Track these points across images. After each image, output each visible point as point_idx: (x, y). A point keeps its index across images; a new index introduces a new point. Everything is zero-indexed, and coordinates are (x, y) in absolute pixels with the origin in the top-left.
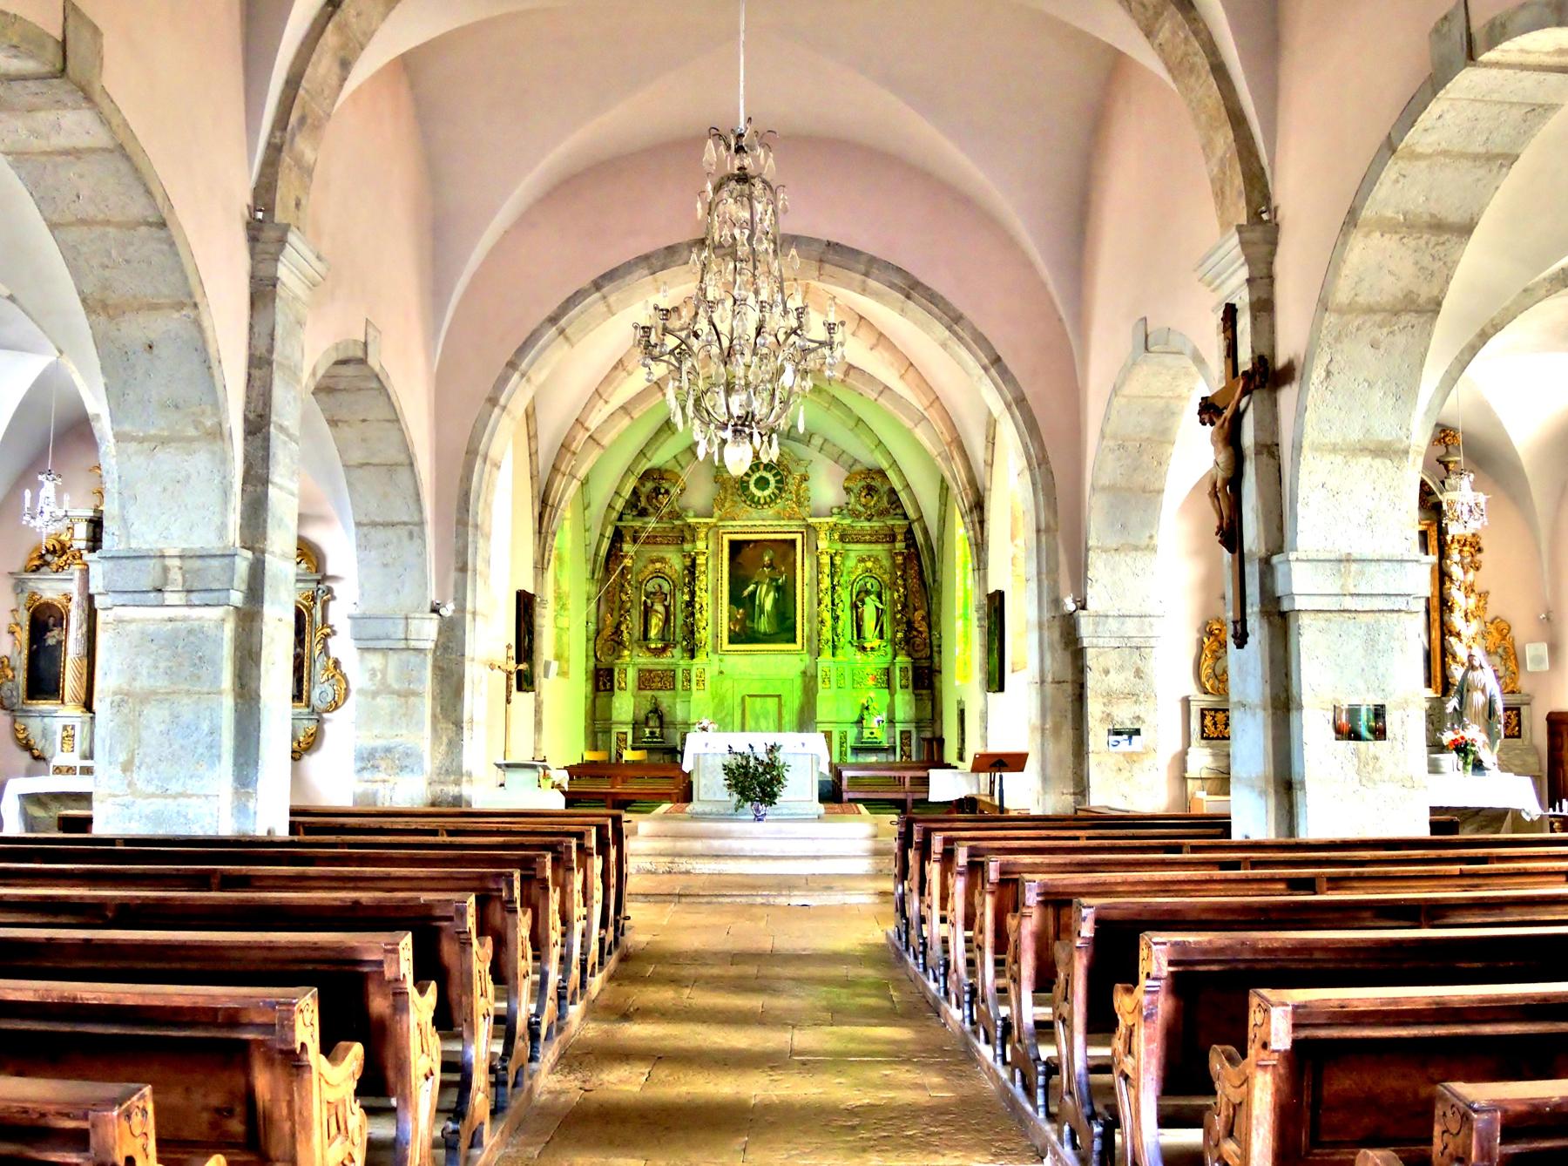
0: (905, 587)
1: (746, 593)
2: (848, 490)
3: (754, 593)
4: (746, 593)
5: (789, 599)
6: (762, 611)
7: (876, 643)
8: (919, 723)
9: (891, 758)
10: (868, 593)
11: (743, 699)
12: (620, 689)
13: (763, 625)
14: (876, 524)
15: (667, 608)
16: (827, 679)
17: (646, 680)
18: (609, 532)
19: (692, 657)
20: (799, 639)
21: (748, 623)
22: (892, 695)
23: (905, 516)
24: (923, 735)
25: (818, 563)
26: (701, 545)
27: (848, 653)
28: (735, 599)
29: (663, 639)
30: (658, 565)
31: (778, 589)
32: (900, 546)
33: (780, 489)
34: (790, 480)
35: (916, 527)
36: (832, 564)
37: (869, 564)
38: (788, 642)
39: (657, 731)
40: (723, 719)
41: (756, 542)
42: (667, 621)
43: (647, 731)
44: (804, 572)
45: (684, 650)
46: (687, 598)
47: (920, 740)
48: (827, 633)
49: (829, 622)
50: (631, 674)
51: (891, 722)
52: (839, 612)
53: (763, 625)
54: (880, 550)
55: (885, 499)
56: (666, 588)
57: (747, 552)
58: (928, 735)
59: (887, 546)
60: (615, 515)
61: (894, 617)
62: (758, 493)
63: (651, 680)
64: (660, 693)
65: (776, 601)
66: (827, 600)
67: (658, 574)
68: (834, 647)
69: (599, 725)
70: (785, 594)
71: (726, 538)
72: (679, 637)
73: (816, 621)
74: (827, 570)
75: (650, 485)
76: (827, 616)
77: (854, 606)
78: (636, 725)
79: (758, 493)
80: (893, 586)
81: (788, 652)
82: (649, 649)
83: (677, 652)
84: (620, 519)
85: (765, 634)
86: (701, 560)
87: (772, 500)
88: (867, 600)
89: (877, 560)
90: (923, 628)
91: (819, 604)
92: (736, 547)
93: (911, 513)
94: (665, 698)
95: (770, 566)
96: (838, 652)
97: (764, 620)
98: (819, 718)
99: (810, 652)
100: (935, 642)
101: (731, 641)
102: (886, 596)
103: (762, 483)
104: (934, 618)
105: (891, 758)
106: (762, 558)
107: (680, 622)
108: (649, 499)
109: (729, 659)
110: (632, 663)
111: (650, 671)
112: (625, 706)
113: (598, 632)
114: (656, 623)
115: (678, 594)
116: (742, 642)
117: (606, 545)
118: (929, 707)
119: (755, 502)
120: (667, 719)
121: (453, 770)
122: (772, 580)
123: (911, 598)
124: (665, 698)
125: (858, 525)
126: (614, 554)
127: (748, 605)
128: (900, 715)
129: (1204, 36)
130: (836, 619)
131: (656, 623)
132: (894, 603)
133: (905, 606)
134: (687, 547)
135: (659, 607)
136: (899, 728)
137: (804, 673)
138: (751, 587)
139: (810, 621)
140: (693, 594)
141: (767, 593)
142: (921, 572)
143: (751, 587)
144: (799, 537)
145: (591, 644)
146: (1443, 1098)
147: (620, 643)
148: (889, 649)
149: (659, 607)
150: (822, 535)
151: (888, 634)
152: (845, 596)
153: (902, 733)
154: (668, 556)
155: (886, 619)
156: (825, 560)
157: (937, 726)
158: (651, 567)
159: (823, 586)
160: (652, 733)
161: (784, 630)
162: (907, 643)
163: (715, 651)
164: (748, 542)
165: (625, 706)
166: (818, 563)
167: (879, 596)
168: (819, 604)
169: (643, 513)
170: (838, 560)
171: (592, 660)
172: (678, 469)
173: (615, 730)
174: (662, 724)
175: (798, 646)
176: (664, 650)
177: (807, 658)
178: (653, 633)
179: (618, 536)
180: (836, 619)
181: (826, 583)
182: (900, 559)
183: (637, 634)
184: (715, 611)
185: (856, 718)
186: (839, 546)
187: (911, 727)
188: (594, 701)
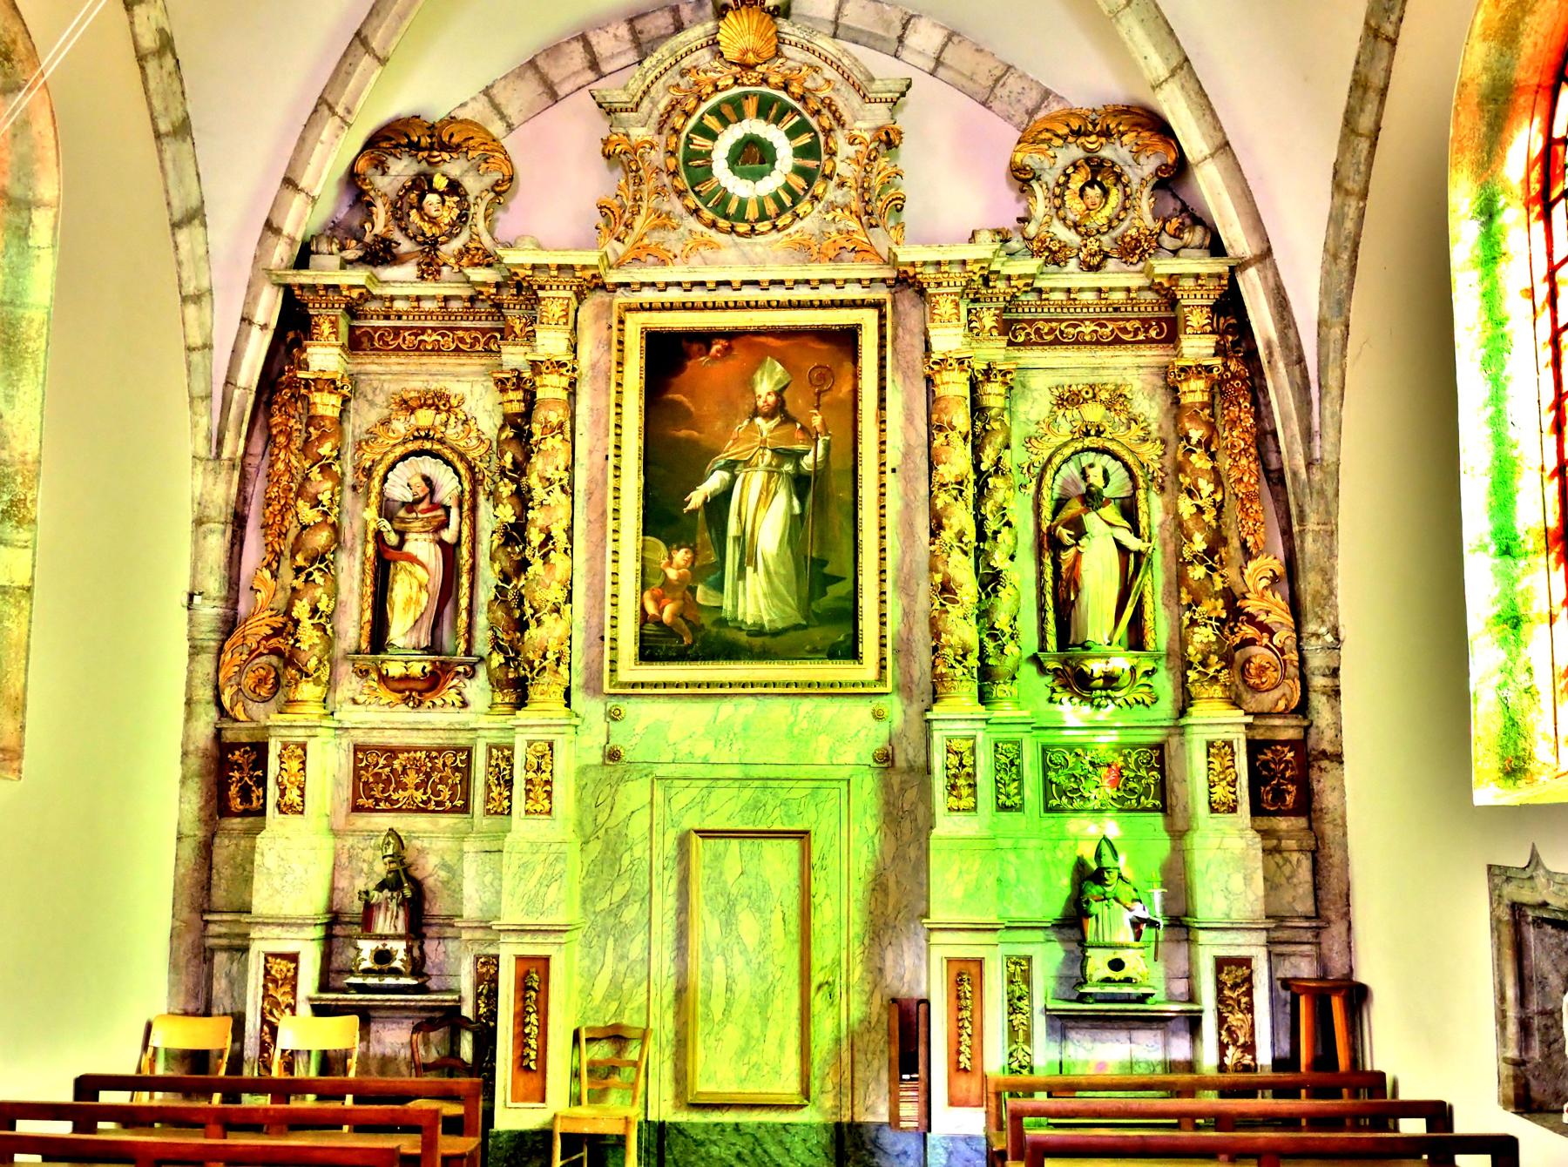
0: (1218, 479)
1: (696, 499)
2: (1022, 178)
3: (719, 505)
4: (696, 499)
5: (839, 520)
6: (747, 558)
7: (1121, 662)
8: (1277, 928)
9: (1180, 1049)
10: (1092, 499)
11: (683, 842)
12: (283, 808)
13: (755, 599)
14: (1119, 277)
15: (449, 552)
16: (962, 777)
17: (376, 780)
18: (268, 307)
19: (521, 702)
20: (869, 646)
21: (703, 595)
22: (1178, 834)
23: (1216, 247)
24: (1286, 970)
25: (932, 400)
26: (551, 343)
27: (1028, 696)
28: (662, 517)
29: (434, 648)
30: (425, 417)
31: (800, 484)
32: (1197, 347)
33: (808, 175)
34: (840, 140)
35: (1252, 287)
36: (977, 409)
37: (1093, 413)
38: (833, 655)
39: (399, 947)
40: (615, 911)
41: (732, 335)
42: (448, 590)
43: (367, 947)
44: (889, 430)
45: (497, 684)
46: (507, 514)
47: (1288, 988)
48: (962, 630)
49: (968, 589)
50: (328, 770)
51: (1180, 924)
52: (999, 560)
53: (755, 599)
54: (1131, 369)
55: (1145, 203)
56: (448, 486)
57: (706, 371)
58: (1305, 969)
59: (1153, 356)
60: (281, 252)
61: (1181, 579)
62: (740, 188)
63: (395, 780)
64: (421, 822)
65: (796, 523)
66: (960, 518)
67: (424, 446)
68: (986, 674)
69: (219, 926)
70: (823, 498)
71: (635, 325)
72: (482, 645)
73: (923, 591)
74: (961, 418)
75: (402, 169)
76: (962, 570)
77: (1048, 544)
78: (336, 927)
79: (740, 188)
80: (1174, 478)
81: (832, 692)
82: (384, 679)
83: (478, 689)
84: (303, 259)
85: (759, 631)
86: (551, 388)
87: (786, 205)
88: (1091, 520)
89: (1117, 400)
90: (1274, 610)
91: (936, 529)
92: (668, 355)
93: (1238, 240)
94: (433, 839)
95: (778, 409)
96: (999, 690)
97: (755, 582)
98: (938, 915)
99: (905, 689)
100: (1317, 660)
101: (648, 652)
102: (1153, 509)
103: (752, 156)
104: (1310, 583)
105: (1180, 1049)
106: (748, 385)
107: (485, 594)
108: (398, 214)
109: (639, 712)
110: (325, 728)
111: (392, 752)
112: (298, 866)
113: (230, 625)
114: (411, 595)
115: (485, 507)
116: (682, 656)
117: (258, 347)
118: (1305, 873)
119: (728, 216)
120: (438, 906)
121: (619, 1012)
122: (781, 454)
123: (1233, 512)
124: (433, 839)
125: (1054, 280)
126: (279, 381)
127: (704, 536)
128: (1209, 905)
129: (682, 917)
130: (990, 581)
131: (411, 595)
132: (1181, 530)
133: (1217, 541)
134: (514, 357)
135: (421, 546)
136: (1209, 948)
137: (886, 760)
138: (715, 482)
139: (906, 588)
140: (523, 499)
141: (767, 495)
142: (1264, 437)
143: (715, 482)
144: (868, 318)
145: (206, 664)
146: (825, 1112)
147: (290, 659)
148: (1164, 684)
149: (421, 546)
150: (945, 307)
151: (1159, 631)
152: (1017, 508)
153: (1221, 963)
154: (453, 388)
155: (1154, 582)
156: (954, 386)
157: (1333, 939)
158: (400, 426)
159: (947, 473)
160: (383, 957)
161: (825, 619)
162: (1228, 660)
163: (593, 686)
164: (704, 338)
165: (298, 866)
166: (932, 400)
167: (1129, 511)
168: (936, 529)
169: (380, 254)
170: (993, 395)
171: (206, 720)
172: (497, 128)
173: (263, 943)
174: (418, 922)
175: (867, 670)
176: (434, 681)
177: (894, 707)
178: (400, 629)
179: (295, 323)
180: (990, 581)
181: (957, 462)
182: (1195, 391)
183: (352, 628)
184: (599, 568)
185: (1054, 906)
186: (993, 351)
187: (1253, 947)
188: (206, 850)
